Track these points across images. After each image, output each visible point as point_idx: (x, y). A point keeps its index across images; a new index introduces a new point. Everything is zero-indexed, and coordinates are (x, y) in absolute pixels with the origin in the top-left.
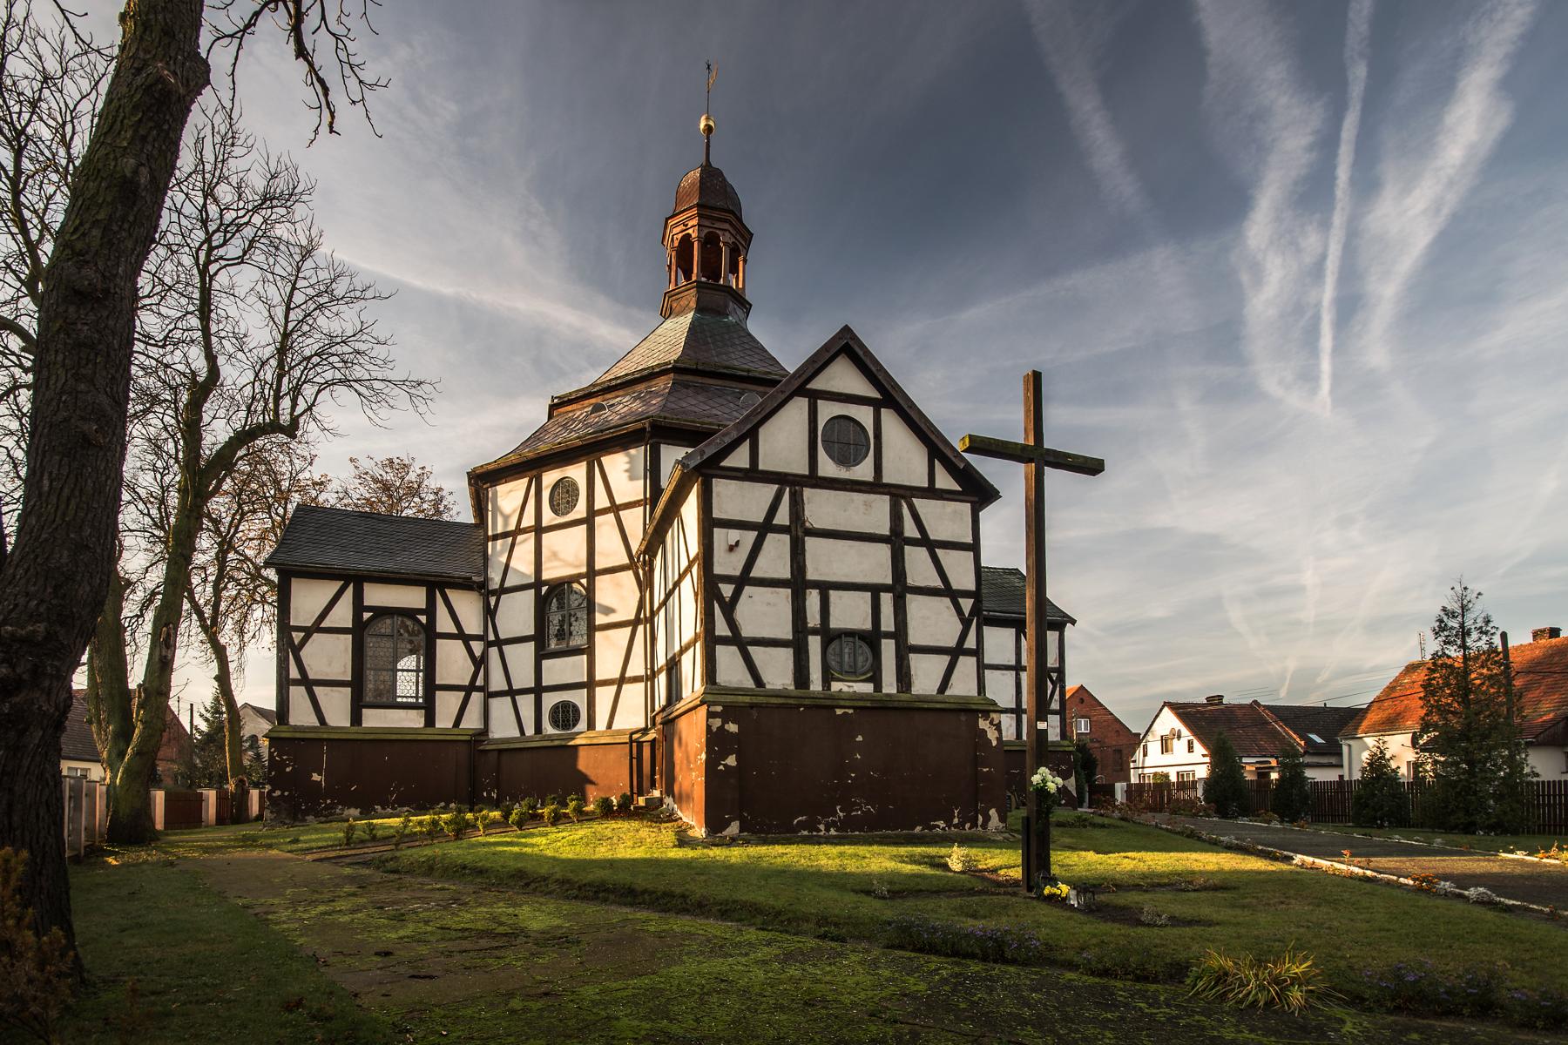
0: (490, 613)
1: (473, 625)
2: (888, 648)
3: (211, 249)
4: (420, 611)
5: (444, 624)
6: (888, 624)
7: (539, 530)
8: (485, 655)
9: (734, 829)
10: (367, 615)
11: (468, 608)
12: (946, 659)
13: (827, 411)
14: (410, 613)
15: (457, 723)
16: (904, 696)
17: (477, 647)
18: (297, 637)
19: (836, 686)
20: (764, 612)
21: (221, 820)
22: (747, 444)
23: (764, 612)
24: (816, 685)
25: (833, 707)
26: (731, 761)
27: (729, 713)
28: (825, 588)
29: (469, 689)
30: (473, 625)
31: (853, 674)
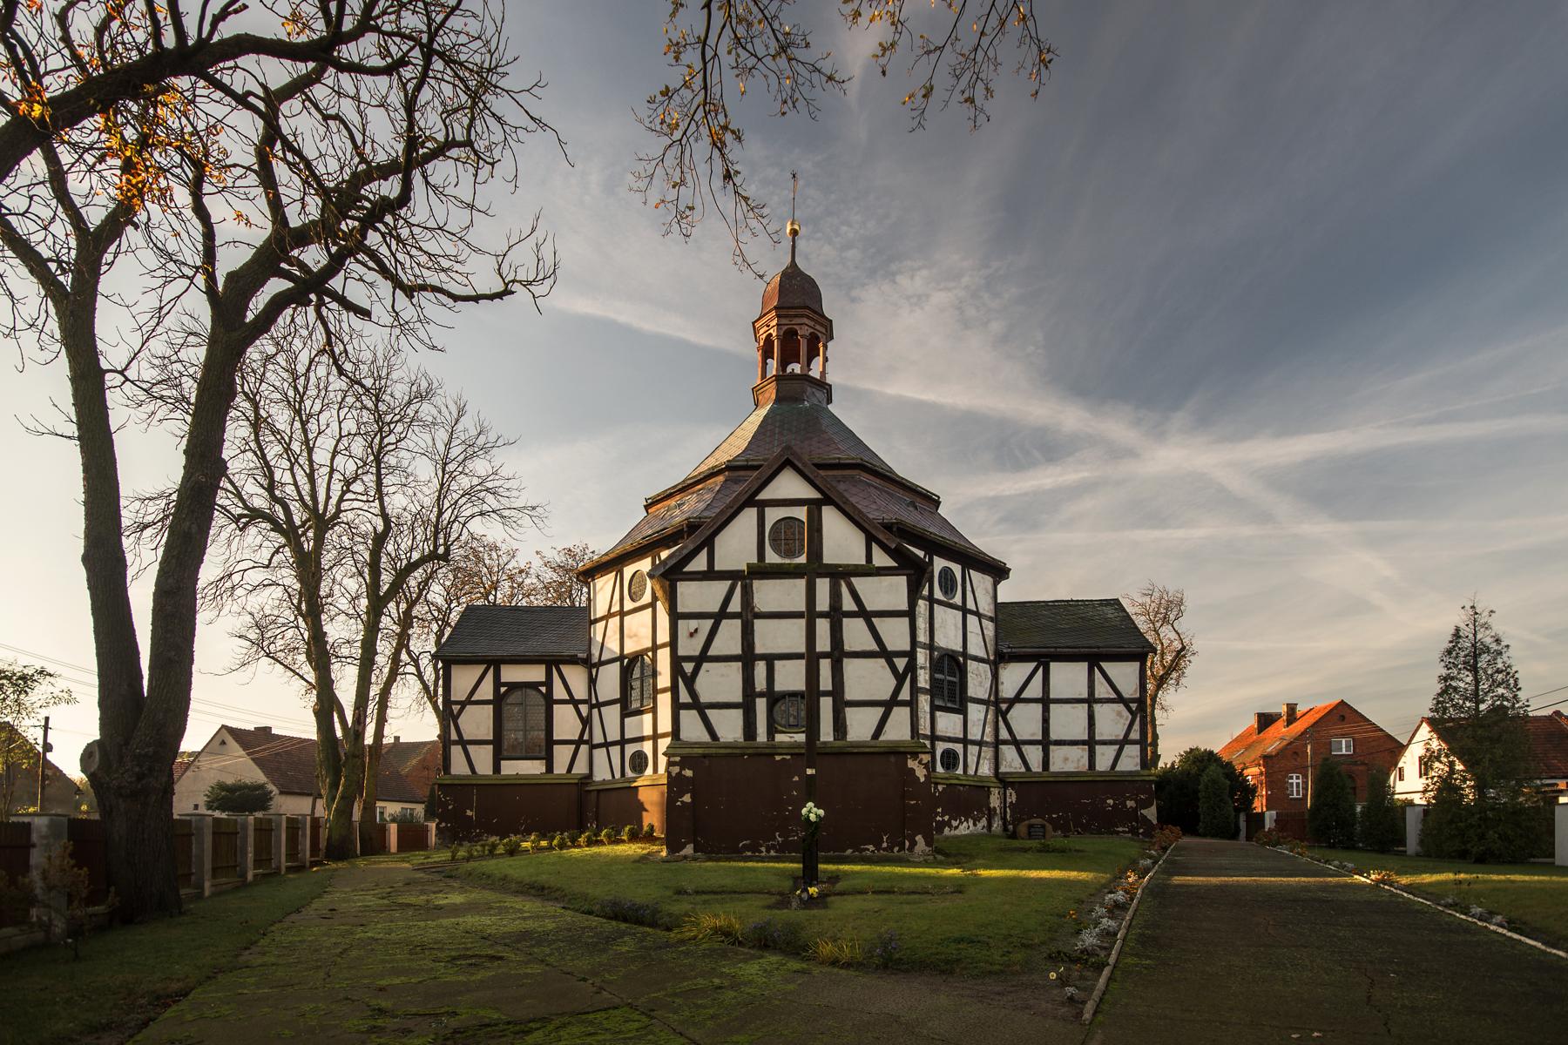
0: (592, 682)
1: (580, 692)
2: (826, 704)
3: (382, 439)
4: (541, 684)
5: (559, 692)
6: (826, 683)
7: (622, 614)
8: (590, 714)
9: (689, 850)
10: (503, 689)
11: (576, 677)
12: (880, 711)
13: (773, 515)
14: (534, 686)
15: (569, 770)
16: (839, 743)
17: (584, 709)
18: (456, 708)
19: (779, 738)
20: (720, 682)
21: (401, 848)
22: (704, 552)
23: (720, 682)
24: (762, 736)
25: (773, 755)
26: (687, 798)
27: (686, 762)
28: (770, 659)
29: (578, 743)
30: (580, 692)
31: (791, 728)
